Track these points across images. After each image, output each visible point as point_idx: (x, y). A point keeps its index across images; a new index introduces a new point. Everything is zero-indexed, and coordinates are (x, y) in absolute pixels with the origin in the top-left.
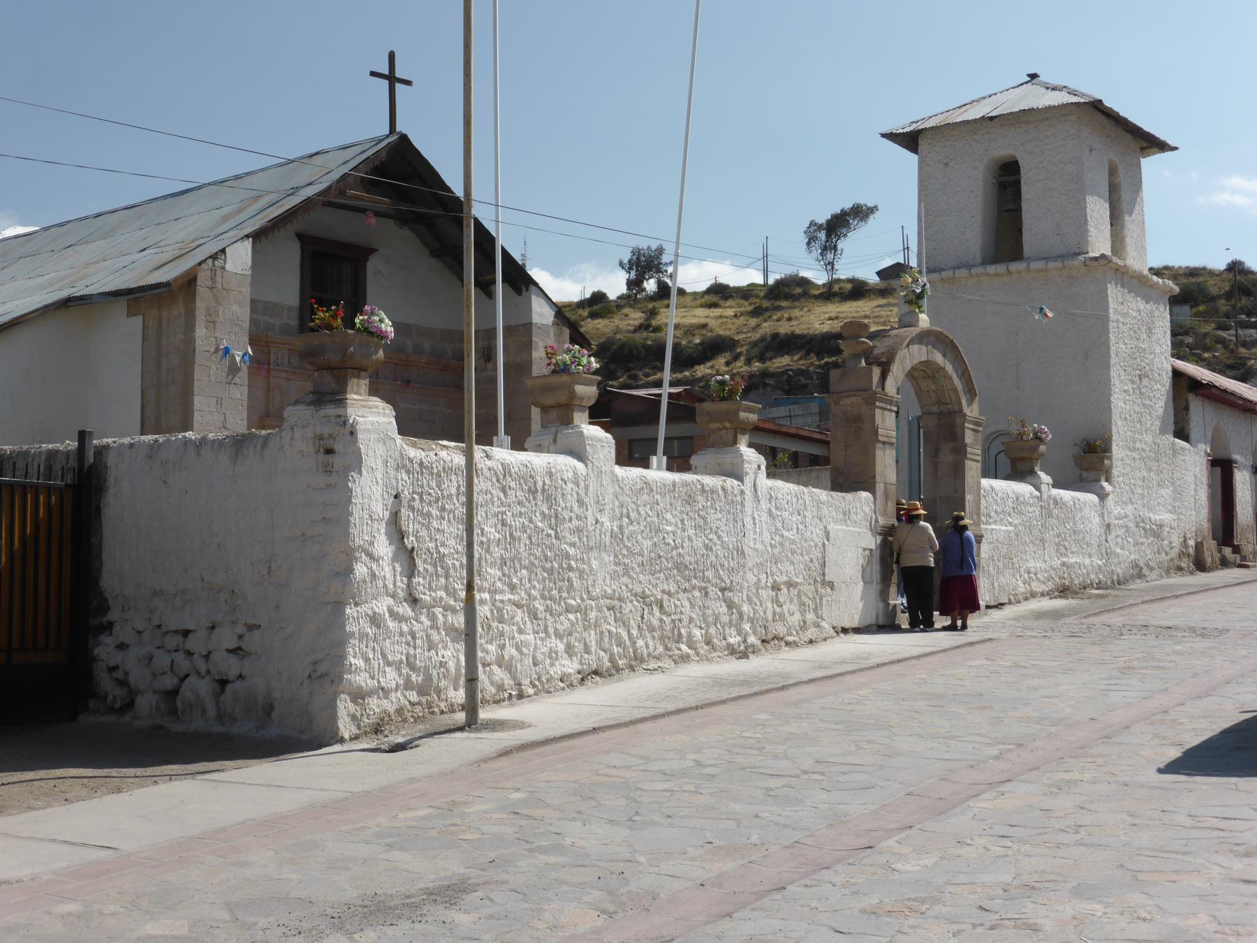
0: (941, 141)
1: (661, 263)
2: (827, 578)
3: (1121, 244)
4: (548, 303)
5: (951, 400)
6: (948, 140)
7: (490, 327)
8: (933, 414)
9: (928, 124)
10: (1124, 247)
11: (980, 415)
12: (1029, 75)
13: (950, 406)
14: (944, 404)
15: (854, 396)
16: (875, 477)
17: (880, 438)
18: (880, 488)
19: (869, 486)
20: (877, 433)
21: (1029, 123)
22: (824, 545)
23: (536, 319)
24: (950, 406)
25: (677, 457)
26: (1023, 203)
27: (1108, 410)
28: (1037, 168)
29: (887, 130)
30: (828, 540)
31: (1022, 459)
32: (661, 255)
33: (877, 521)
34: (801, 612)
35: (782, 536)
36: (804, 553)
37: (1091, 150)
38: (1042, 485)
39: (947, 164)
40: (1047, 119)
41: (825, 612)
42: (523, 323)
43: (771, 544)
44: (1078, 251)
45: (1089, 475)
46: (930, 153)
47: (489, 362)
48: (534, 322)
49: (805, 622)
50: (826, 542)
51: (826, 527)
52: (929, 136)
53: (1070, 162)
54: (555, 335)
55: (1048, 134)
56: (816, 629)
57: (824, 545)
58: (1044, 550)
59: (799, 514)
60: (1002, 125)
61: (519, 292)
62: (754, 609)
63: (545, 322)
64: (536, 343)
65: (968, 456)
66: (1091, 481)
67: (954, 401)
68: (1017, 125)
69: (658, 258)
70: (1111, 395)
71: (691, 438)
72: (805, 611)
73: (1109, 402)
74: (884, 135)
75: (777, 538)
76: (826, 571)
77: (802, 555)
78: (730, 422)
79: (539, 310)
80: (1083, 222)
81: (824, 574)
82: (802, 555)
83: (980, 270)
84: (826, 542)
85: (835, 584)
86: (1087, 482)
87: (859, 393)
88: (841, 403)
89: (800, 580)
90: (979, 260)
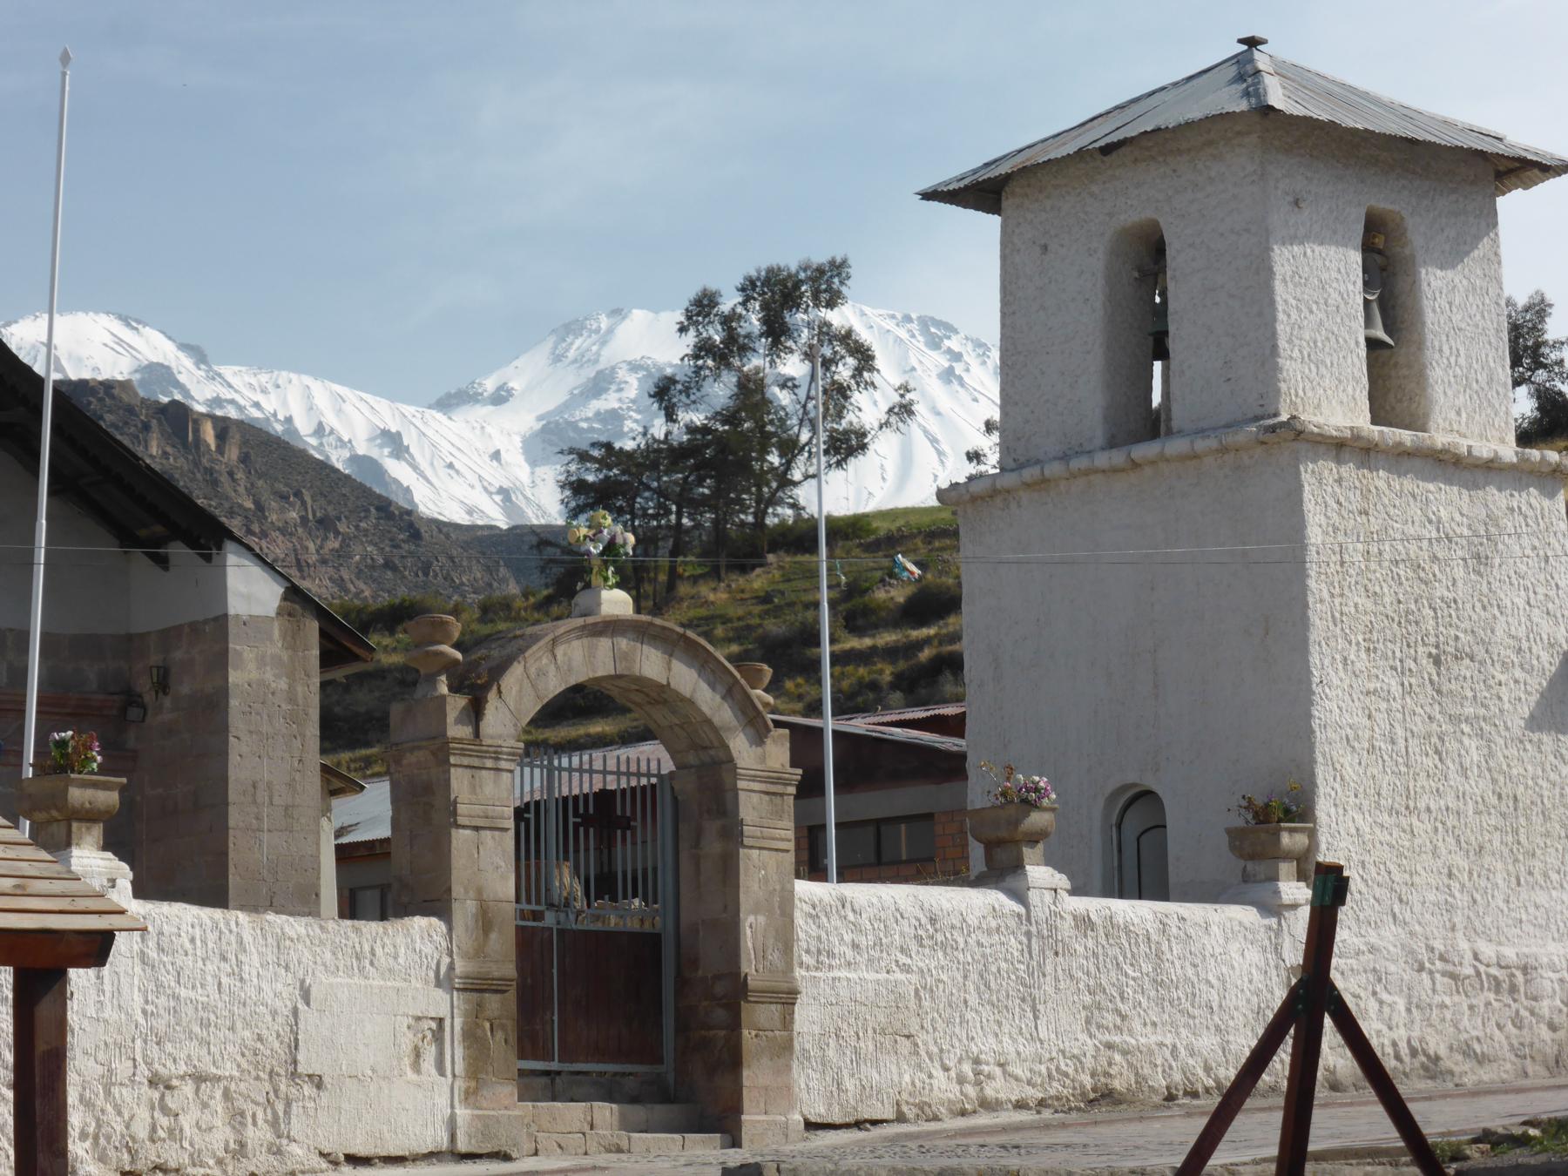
0: (1037, 200)
1: (1545, 343)
2: (300, 1069)
3: (1418, 383)
4: (265, 575)
5: (711, 742)
6: (1048, 197)
7: (220, 613)
8: (692, 766)
9: (1004, 169)
10: (1424, 389)
11: (792, 766)
12: (1241, 41)
13: (712, 752)
14: (705, 748)
15: (419, 748)
16: (449, 890)
17: (461, 820)
18: (464, 908)
19: (435, 903)
20: (455, 813)
21: (1180, 152)
22: (295, 1011)
23: (236, 606)
24: (712, 752)
25: (909, 862)
26: (1170, 318)
27: (1303, 735)
28: (1191, 245)
29: (927, 184)
30: (308, 1004)
31: (1000, 843)
32: (1542, 321)
33: (451, 967)
34: (234, 1128)
35: (176, 998)
36: (239, 1025)
37: (1296, 203)
38: (1030, 893)
39: (1045, 248)
40: (1210, 143)
41: (297, 1126)
42: (211, 616)
43: (144, 1012)
44: (1259, 411)
45: (1260, 868)
46: (1019, 224)
47: (165, 693)
48: (232, 611)
49: (242, 1145)
50: (301, 1006)
51: (303, 982)
52: (1017, 190)
53: (1247, 231)
54: (284, 636)
55: (1213, 174)
56: (271, 1158)
57: (295, 1011)
58: (1036, 1018)
59: (224, 959)
60: (1136, 161)
61: (208, 558)
62: (98, 1120)
63: (257, 611)
64: (240, 654)
65: (746, 841)
66: (1260, 881)
67: (716, 743)
68: (1161, 159)
69: (1534, 328)
70: (1311, 703)
71: (929, 816)
72: (244, 1125)
73: (1309, 716)
74: (930, 195)
75: (162, 1001)
76: (300, 1057)
77: (232, 1028)
78: (58, 810)
79: (242, 588)
80: (1268, 352)
81: (295, 1062)
82: (232, 1028)
83: (1102, 460)
84: (301, 1006)
85: (326, 1079)
86: (1255, 882)
87: (424, 743)
88: (405, 762)
89: (229, 1069)
90: (1099, 440)
